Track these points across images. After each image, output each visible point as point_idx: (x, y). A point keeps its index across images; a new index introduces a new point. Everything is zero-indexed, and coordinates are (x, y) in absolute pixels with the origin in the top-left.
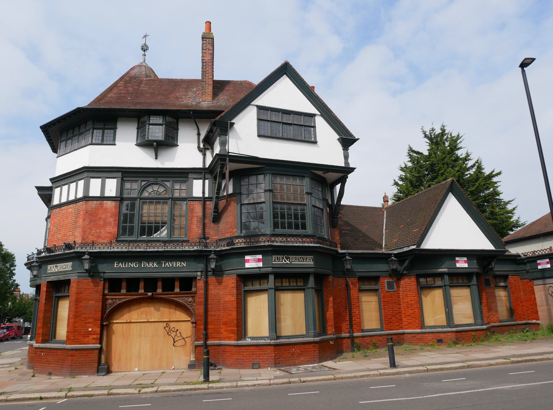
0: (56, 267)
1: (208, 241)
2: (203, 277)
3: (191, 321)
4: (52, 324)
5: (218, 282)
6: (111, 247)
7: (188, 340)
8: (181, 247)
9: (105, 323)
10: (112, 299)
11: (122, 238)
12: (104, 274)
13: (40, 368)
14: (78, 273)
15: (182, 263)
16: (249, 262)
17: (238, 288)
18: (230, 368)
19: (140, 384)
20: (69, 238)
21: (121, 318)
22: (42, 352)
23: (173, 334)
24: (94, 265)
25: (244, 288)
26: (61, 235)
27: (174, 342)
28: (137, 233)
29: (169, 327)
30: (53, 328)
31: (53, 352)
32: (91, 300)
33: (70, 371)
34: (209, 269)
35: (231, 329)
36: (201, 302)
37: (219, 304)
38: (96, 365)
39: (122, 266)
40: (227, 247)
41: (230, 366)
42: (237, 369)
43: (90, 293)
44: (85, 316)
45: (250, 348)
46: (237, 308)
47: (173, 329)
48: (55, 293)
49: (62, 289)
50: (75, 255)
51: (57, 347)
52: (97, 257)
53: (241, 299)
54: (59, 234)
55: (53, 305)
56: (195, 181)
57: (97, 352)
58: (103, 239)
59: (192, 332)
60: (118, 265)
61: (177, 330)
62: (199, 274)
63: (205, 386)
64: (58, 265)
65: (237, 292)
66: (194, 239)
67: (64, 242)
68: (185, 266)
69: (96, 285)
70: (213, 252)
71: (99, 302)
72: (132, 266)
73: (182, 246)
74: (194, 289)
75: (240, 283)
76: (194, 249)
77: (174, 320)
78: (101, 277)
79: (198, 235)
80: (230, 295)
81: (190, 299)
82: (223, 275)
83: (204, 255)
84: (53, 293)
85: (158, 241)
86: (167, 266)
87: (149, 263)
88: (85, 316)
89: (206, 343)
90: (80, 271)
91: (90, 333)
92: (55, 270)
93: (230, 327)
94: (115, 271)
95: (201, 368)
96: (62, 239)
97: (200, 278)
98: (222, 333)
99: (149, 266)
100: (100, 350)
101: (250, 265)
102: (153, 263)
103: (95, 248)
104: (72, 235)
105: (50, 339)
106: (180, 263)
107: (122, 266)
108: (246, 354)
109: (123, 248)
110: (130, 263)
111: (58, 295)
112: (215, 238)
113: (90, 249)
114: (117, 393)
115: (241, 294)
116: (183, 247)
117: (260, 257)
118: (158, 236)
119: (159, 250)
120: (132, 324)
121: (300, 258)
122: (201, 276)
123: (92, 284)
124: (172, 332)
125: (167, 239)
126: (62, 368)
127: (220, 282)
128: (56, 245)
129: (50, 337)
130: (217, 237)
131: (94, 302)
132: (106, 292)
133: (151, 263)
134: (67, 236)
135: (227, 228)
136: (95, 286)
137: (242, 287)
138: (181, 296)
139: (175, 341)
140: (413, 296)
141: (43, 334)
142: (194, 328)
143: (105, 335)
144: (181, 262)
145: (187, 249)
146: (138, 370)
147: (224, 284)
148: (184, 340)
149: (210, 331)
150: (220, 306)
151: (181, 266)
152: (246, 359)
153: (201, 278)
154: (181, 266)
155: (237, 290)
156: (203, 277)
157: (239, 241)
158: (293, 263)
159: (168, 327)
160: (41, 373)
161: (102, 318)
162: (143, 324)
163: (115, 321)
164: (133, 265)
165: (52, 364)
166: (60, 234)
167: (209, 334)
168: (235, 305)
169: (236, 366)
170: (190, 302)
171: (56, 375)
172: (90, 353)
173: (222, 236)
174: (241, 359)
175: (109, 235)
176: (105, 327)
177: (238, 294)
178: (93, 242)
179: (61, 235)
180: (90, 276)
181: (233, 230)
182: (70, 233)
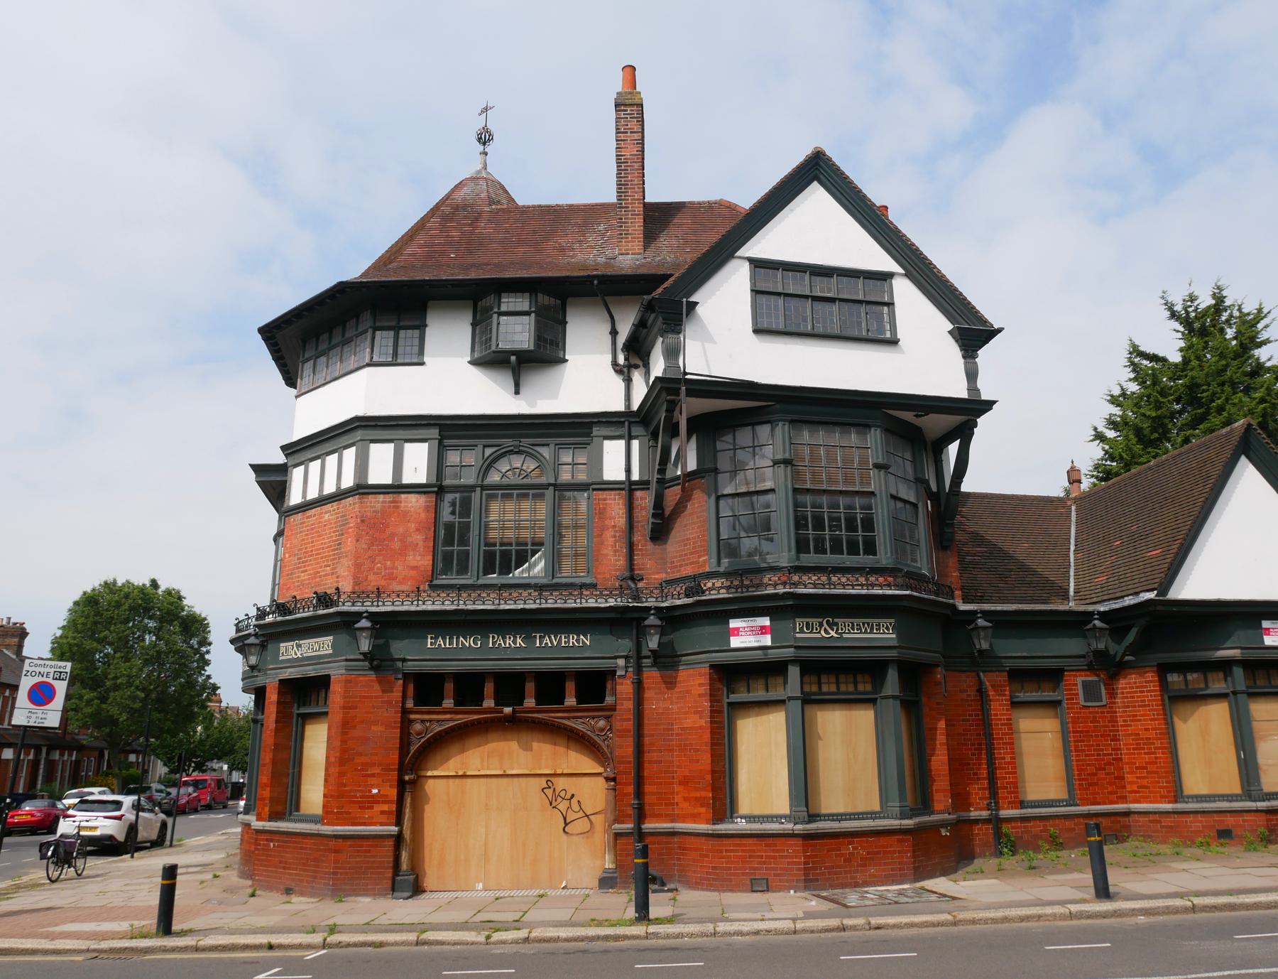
0: (299, 646)
1: (640, 585)
3: (605, 775)
5: (665, 683)
6: (418, 600)
7: (598, 820)
8: (578, 601)
9: (407, 778)
10: (423, 721)
11: (443, 580)
14: (347, 660)
15: (582, 637)
16: (738, 635)
17: (714, 697)
18: (698, 889)
20: (326, 580)
23: (563, 806)
24: (381, 641)
27: (566, 824)
31: (295, 842)
34: (645, 652)
35: (698, 794)
36: (629, 731)
38: (389, 874)
39: (445, 645)
40: (686, 599)
41: (697, 883)
42: (714, 891)
44: (363, 759)
46: (713, 744)
47: (563, 794)
48: (296, 705)
49: (312, 698)
52: (388, 624)
53: (722, 722)
54: (303, 572)
56: (607, 444)
57: (391, 843)
58: (401, 583)
60: (435, 643)
62: (621, 662)
64: (301, 642)
65: (711, 707)
66: (608, 580)
67: (314, 590)
68: (588, 643)
69: (387, 687)
70: (652, 612)
72: (467, 645)
73: (581, 598)
74: (609, 700)
75: (719, 685)
76: (608, 605)
78: (397, 671)
79: (616, 570)
80: (696, 712)
81: (602, 723)
83: (632, 619)
86: (547, 643)
87: (504, 638)
88: (363, 759)
89: (640, 829)
91: (375, 800)
92: (296, 654)
93: (696, 789)
94: (428, 657)
95: (628, 887)
101: (742, 642)
104: (333, 574)
106: (575, 637)
107: (445, 645)
110: (461, 639)
112: (656, 577)
113: (372, 606)
115: (721, 712)
116: (583, 601)
117: (766, 621)
119: (527, 607)
120: (469, 781)
122: (626, 667)
123: (377, 687)
124: (559, 799)
125: (545, 581)
126: (315, 877)
128: (298, 598)
129: (288, 806)
131: (382, 728)
132: (410, 704)
133: (510, 638)
135: (686, 555)
136: (383, 691)
139: (568, 821)
140: (1151, 720)
141: (271, 798)
142: (612, 793)
143: (408, 805)
144: (578, 636)
145: (592, 603)
146: (484, 887)
148: (589, 819)
149: (648, 799)
152: (735, 868)
153: (626, 672)
155: (711, 701)
156: (630, 669)
157: (713, 584)
158: (845, 636)
159: (550, 788)
160: (269, 888)
161: (401, 763)
163: (429, 773)
164: (469, 642)
166: (306, 571)
167: (647, 808)
169: (711, 885)
170: (602, 730)
171: (302, 894)
172: (377, 846)
173: (673, 572)
174: (722, 868)
175: (413, 573)
176: (408, 786)
177: (715, 712)
180: (372, 668)
181: (699, 557)
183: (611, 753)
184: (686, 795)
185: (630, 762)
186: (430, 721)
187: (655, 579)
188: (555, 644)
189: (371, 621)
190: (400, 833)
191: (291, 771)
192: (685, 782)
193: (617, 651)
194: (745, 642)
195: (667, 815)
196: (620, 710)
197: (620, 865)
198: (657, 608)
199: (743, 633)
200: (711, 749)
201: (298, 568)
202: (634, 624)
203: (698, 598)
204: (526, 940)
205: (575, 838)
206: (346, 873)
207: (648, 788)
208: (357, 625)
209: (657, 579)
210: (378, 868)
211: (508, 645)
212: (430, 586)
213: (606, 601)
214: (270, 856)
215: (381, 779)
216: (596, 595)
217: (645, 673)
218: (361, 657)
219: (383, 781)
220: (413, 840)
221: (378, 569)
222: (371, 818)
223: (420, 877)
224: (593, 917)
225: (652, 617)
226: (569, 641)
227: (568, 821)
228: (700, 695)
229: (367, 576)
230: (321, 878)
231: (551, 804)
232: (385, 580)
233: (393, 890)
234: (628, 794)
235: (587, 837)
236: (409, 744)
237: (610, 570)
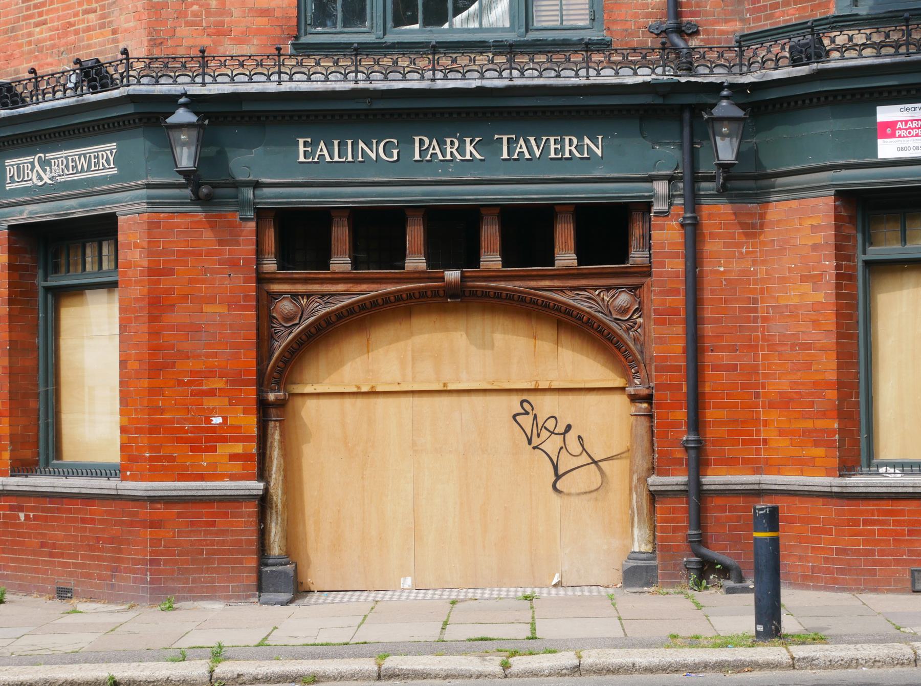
0: (44, 163)
1: (694, 42)
2: (679, 201)
3: (631, 390)
4: (41, 397)
5: (743, 225)
6: (280, 73)
7: (616, 470)
8: (583, 72)
9: (272, 397)
10: (295, 296)
11: (318, 35)
12: (258, 192)
13: (15, 569)
14: (149, 186)
15: (587, 141)
16: (893, 135)
17: (842, 251)
18: (808, 588)
19: (482, 639)
20: (90, 38)
21: (335, 377)
22: (21, 509)
23: (552, 445)
24: (211, 151)
25: (864, 253)
26: (50, 30)
27: (558, 477)
28: (380, 13)
29: (535, 416)
30: (47, 417)
31: (69, 511)
32: (211, 300)
33: (151, 582)
34: (705, 168)
35: (809, 425)
36: (676, 312)
37: (748, 320)
38: (251, 561)
39: (331, 157)
40: (791, 69)
41: (805, 577)
42: (842, 590)
43: (204, 271)
44: (191, 364)
45: (864, 506)
46: (840, 336)
47: (550, 424)
48: (40, 273)
49: (88, 251)
50: (129, 109)
51: (84, 491)
53: (854, 297)
54: (37, 25)
55: (41, 322)
57: (251, 509)
58: (240, 41)
59: (633, 436)
60: (313, 153)
61: (569, 427)
62: (661, 188)
63: (771, 652)
64: (49, 156)
65: (838, 267)
66: (631, 34)
67: (75, 55)
68: (599, 152)
69: (228, 235)
70: (725, 93)
71: (246, 308)
72: (373, 156)
73: (588, 68)
74: (637, 256)
75: (849, 230)
76: (639, 80)
77: (555, 385)
78: (243, 205)
79: (648, 15)
80: (804, 279)
81: (623, 299)
82: (769, 193)
83: (683, 107)
84: (34, 276)
85: (479, 46)
87: (441, 144)
88: (191, 364)
89: (699, 484)
90: (157, 180)
91: (217, 436)
92: (41, 179)
93: (804, 416)
94: (301, 179)
95: (680, 583)
96: (53, 46)
97: (665, 208)
98: (765, 441)
99: (444, 155)
100: (263, 501)
101: (902, 149)
102: (462, 143)
103: (214, 78)
104: (102, 26)
105: (42, 458)
106: (575, 141)
107: (331, 157)
108: (882, 533)
109: (297, 77)
110: (361, 145)
111: (54, 282)
112: (724, 27)
113: (193, 82)
114: (414, 671)
115: (851, 278)
116: (592, 72)
118: (474, 25)
119: (488, 83)
120: (381, 401)
121: (80, 156)
122: (671, 197)
123: (208, 234)
124: (545, 434)
125: (512, 37)
126: (116, 569)
127: (753, 226)
128: (39, 72)
129: (42, 450)
130: (737, 27)
131: (222, 309)
132: (270, 265)
133: (452, 143)
134: (77, 32)
136: (221, 243)
137: (855, 246)
138: (583, 282)
139: (561, 471)
141: (13, 438)
142: (644, 423)
143: (276, 444)
144: (580, 139)
145: (608, 77)
146: (414, 583)
147: (769, 235)
148: (599, 468)
149: (712, 433)
150: (755, 329)
151: (581, 153)
152: (882, 553)
153: (671, 205)
154: (581, 153)
155: (838, 258)
156: (679, 201)
157: (851, 39)
159: (527, 413)
160: (26, 590)
161: (261, 373)
162: (426, 401)
163: (309, 389)
164: (376, 151)
165: (70, 556)
166: (44, 23)
167: (710, 448)
168: (829, 321)
169: (835, 581)
170: (624, 311)
171: (92, 598)
172: (226, 515)
173: (758, 19)
174: (857, 552)
175: (261, 22)
176: (273, 412)
177: (843, 277)
178: (203, 52)
179: (50, 30)
180: (198, 200)
182: (92, 16)
183: (641, 352)
184: (785, 426)
185: (678, 369)
186: (308, 296)
187: (722, 32)
188: (538, 154)
189: (197, 113)
190: (266, 490)
191: (41, 389)
192: (783, 403)
193: (654, 167)
194: (908, 149)
195: (746, 461)
196: (660, 275)
197: (659, 545)
198: (732, 86)
199: (903, 133)
200: (837, 343)
201: (26, 18)
202: (687, 116)
203: (820, 66)
204: (577, 670)
205: (575, 501)
206: (175, 562)
207: (711, 414)
208: (171, 120)
209: (727, 33)
210: (232, 552)
211: (448, 157)
212: (297, 47)
213: (635, 74)
214: (20, 535)
215: (226, 399)
216: (634, 63)
217: (704, 207)
218: (181, 180)
219: (231, 404)
220: (286, 505)
221: (195, 14)
222: (214, 466)
223: (299, 567)
224: (674, 632)
225: (724, 103)
226: (563, 148)
227: (560, 472)
228: (815, 247)
229: (174, 29)
230: (126, 570)
231: (530, 442)
232: (209, 35)
233: (260, 589)
234: (675, 425)
235: (596, 499)
236: (272, 337)
237: (636, 15)
